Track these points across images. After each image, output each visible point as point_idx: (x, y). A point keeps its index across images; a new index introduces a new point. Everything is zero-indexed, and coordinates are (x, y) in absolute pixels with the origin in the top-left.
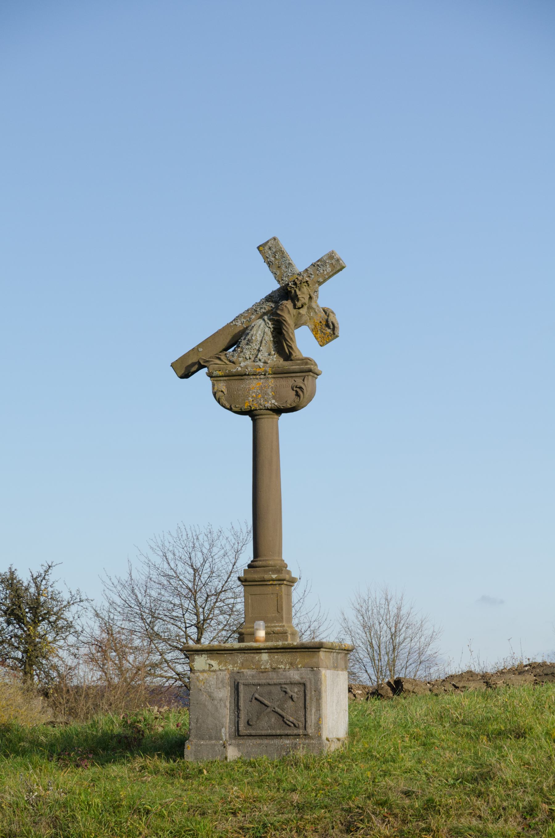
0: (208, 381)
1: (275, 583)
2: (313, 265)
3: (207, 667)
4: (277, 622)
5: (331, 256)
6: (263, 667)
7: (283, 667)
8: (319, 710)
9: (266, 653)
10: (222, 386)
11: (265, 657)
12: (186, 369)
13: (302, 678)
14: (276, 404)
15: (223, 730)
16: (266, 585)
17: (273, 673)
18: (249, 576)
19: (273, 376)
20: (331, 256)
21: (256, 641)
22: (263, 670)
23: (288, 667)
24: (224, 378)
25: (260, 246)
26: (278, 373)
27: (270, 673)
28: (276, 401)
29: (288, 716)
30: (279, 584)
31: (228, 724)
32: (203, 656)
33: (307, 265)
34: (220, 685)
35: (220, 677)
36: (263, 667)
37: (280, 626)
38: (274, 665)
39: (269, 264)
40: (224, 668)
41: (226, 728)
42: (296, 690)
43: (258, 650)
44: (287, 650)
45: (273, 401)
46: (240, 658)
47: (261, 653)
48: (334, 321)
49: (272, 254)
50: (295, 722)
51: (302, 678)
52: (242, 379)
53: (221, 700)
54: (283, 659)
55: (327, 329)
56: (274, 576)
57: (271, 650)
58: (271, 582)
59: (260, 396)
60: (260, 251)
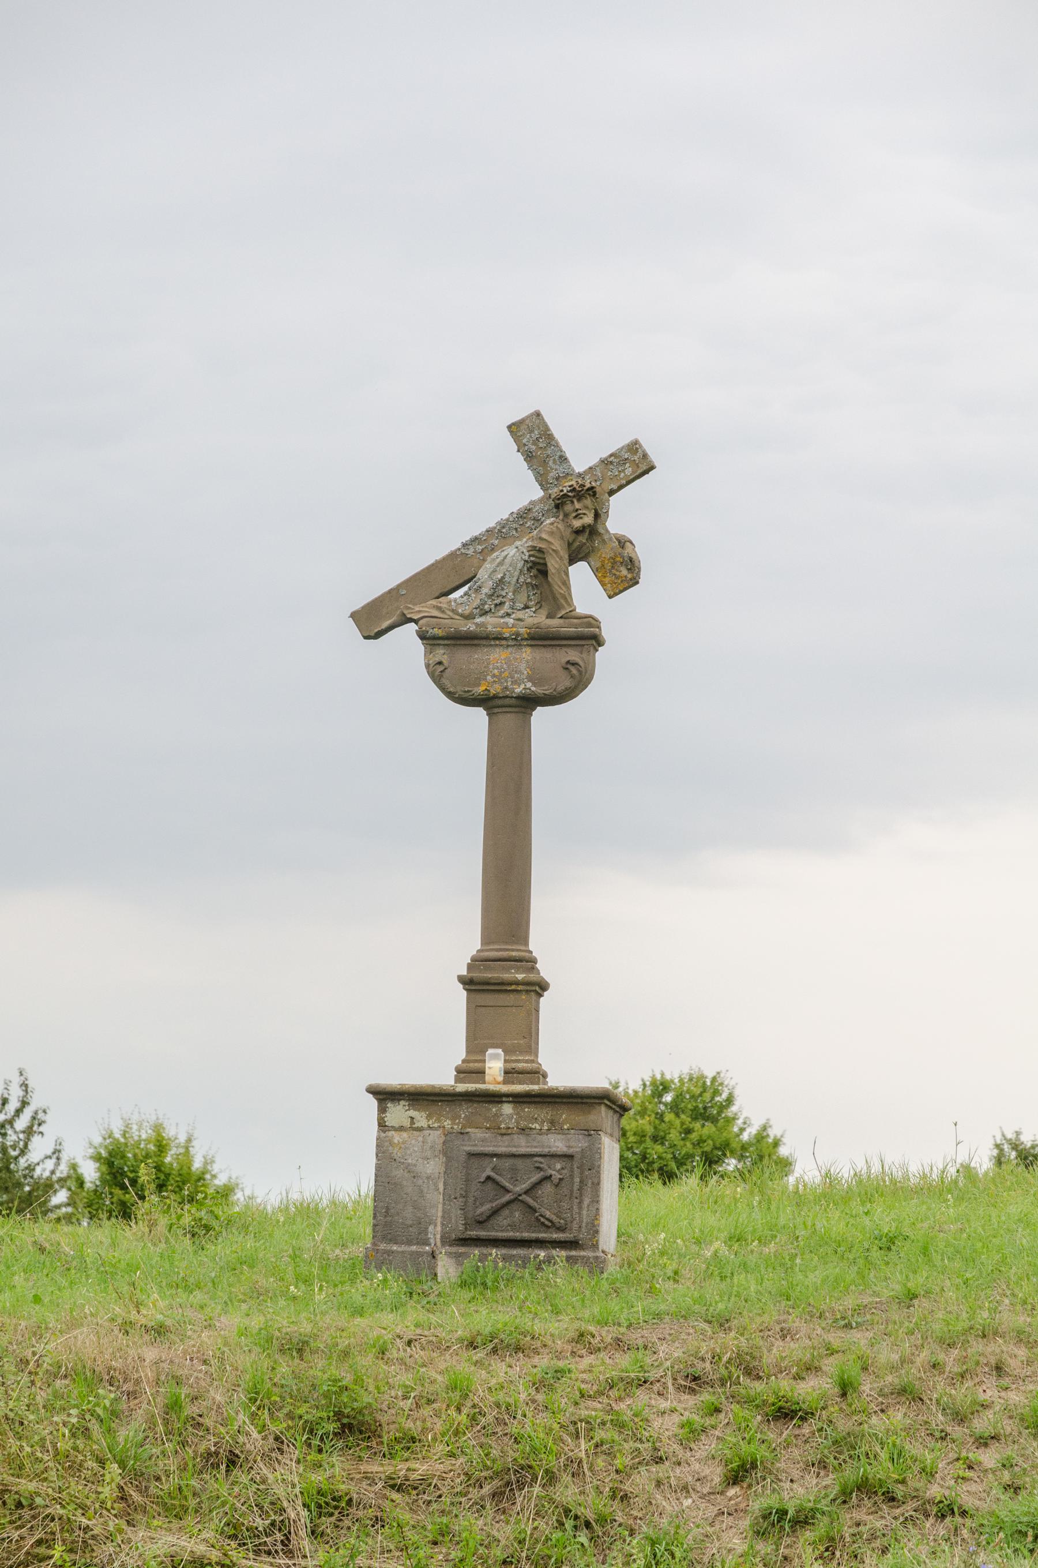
0: (418, 647)
1: (520, 988)
2: (602, 461)
3: (407, 1123)
4: (521, 1053)
5: (634, 447)
6: (503, 1126)
7: (538, 1127)
8: (598, 1202)
9: (509, 1102)
10: (441, 654)
11: (507, 1109)
12: (374, 620)
13: (569, 1147)
14: (533, 689)
15: (431, 1228)
16: (506, 991)
17: (520, 1136)
18: (476, 975)
19: (529, 642)
20: (634, 447)
21: (484, 1082)
22: (503, 1131)
23: (546, 1128)
24: (446, 642)
25: (513, 424)
26: (541, 639)
27: (515, 1136)
28: (534, 684)
29: (543, 1209)
30: (527, 991)
31: (439, 1220)
32: (402, 1103)
33: (594, 461)
34: (429, 1154)
35: (430, 1139)
36: (503, 1126)
37: (527, 1061)
38: (523, 1124)
39: (529, 457)
40: (436, 1125)
41: (436, 1225)
42: (558, 1166)
43: (494, 1098)
44: (533, 1099)
45: (529, 685)
46: (464, 1111)
47: (502, 1102)
48: (633, 555)
49: (534, 439)
50: (554, 1218)
51: (569, 1147)
52: (475, 645)
53: (428, 1178)
54: (538, 1117)
55: (622, 572)
56: (520, 977)
57: (518, 1099)
58: (513, 987)
59: (506, 674)
60: (511, 432)
